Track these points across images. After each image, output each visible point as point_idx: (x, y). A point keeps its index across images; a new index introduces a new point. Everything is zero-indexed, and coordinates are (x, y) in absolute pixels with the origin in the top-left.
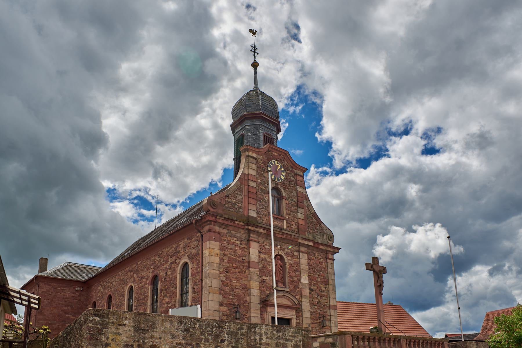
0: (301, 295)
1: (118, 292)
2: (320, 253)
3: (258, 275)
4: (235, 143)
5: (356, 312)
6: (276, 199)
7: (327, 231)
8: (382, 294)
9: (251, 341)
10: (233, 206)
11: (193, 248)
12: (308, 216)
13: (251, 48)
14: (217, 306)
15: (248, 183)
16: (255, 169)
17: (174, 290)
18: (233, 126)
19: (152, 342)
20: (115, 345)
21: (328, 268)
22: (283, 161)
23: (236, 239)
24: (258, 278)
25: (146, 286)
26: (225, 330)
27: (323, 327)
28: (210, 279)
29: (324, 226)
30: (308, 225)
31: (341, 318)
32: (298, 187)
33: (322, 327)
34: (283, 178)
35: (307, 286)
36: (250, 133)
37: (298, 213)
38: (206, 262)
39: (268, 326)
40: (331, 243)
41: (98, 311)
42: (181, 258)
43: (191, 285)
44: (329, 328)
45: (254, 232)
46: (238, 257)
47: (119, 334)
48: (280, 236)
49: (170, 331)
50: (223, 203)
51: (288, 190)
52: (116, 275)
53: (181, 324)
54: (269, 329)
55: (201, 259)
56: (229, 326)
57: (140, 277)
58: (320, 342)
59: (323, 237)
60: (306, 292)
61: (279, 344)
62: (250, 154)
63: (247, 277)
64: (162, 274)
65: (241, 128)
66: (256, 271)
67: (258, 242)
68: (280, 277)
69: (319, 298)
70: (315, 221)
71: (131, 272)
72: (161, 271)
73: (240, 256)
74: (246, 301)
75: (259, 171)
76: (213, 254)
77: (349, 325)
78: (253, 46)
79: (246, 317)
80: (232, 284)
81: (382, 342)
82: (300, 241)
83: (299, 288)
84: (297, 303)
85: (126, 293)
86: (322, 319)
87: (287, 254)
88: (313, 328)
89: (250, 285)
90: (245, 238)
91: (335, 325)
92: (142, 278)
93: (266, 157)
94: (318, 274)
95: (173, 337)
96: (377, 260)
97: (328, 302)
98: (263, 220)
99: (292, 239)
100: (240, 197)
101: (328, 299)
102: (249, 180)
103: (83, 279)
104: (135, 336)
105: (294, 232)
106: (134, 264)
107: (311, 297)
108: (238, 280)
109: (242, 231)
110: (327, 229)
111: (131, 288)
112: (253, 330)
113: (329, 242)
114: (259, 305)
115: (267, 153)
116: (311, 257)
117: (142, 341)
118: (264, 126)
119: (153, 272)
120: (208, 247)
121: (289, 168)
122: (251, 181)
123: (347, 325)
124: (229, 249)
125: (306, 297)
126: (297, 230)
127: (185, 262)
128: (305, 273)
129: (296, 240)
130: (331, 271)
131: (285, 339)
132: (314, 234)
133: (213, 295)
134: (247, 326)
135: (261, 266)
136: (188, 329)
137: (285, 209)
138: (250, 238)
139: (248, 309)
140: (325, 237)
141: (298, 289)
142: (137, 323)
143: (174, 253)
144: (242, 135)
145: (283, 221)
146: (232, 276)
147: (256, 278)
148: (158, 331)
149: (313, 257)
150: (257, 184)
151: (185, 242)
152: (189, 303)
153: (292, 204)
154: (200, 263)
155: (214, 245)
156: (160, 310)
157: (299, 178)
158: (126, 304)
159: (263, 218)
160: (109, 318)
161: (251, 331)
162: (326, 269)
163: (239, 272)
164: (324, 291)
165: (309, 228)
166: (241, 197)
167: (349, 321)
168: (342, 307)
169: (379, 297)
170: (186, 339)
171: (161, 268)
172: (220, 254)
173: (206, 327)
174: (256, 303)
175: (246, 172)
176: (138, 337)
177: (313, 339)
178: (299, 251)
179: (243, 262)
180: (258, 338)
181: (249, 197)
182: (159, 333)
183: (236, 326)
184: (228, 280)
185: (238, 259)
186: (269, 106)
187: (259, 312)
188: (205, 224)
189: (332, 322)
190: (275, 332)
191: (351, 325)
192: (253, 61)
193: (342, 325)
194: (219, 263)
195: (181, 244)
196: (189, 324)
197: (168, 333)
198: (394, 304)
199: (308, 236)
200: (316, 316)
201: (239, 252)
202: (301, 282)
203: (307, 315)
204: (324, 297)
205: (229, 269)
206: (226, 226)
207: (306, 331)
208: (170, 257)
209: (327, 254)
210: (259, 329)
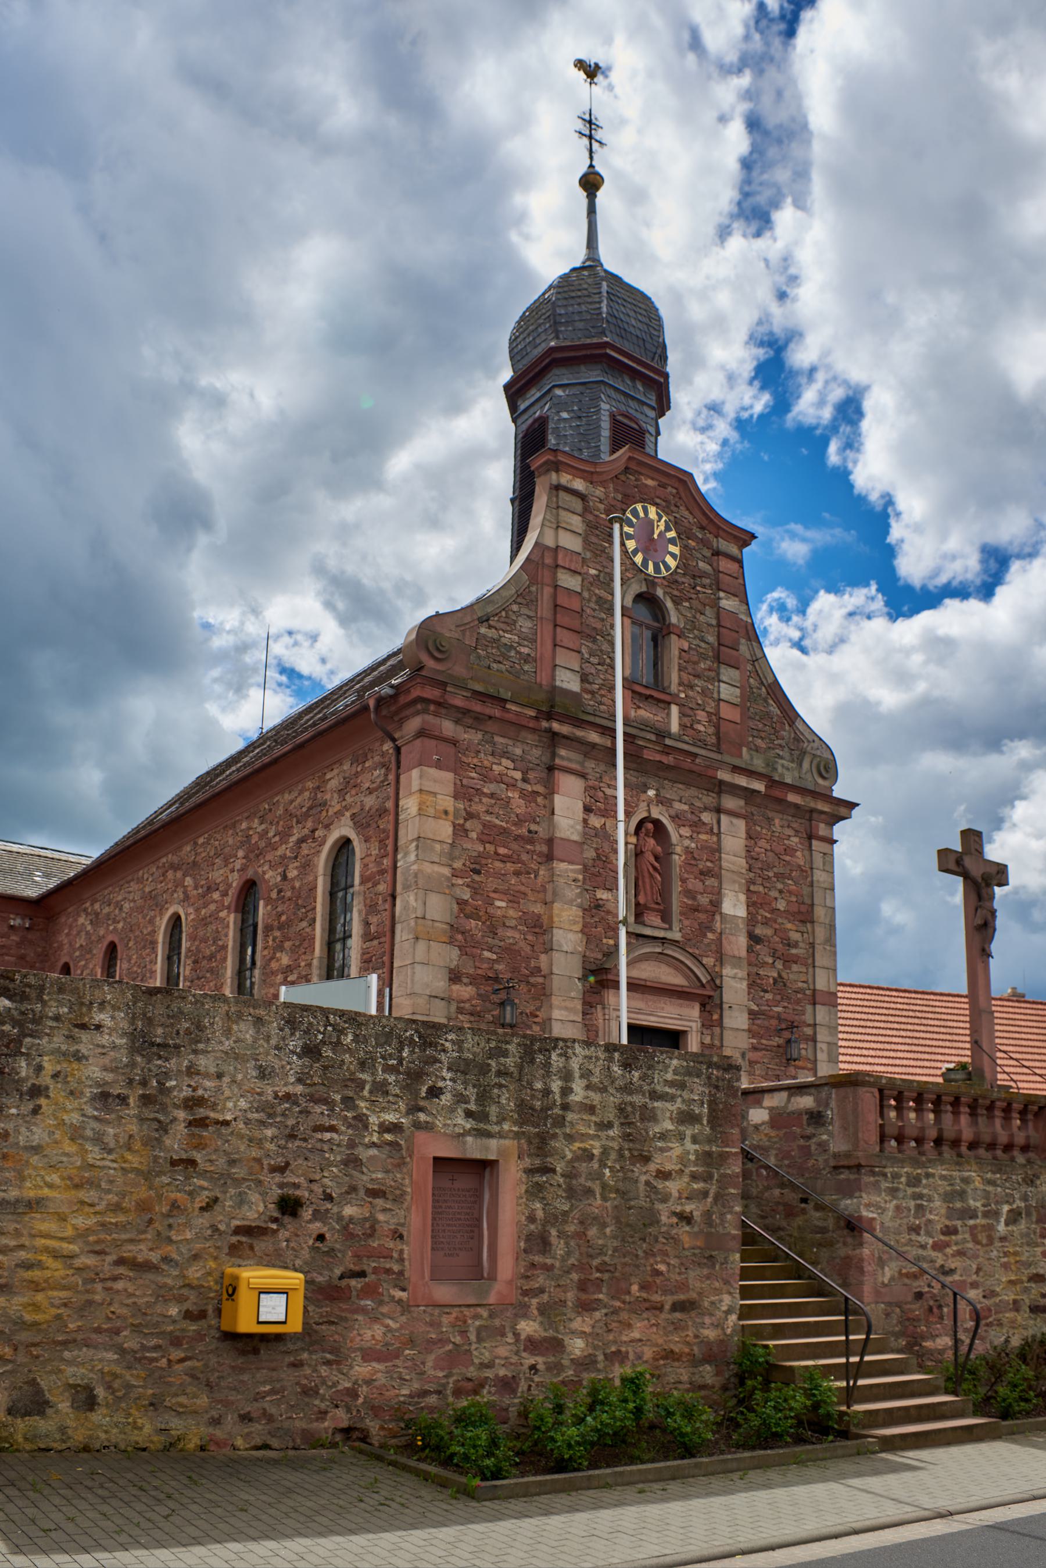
0: (722, 954)
1: (137, 933)
2: (790, 818)
3: (579, 884)
4: (519, 445)
5: (903, 1020)
6: (648, 634)
7: (815, 745)
8: (990, 955)
9: (533, 1097)
10: (503, 655)
11: (370, 791)
12: (753, 693)
13: (580, 125)
14: (442, 983)
15: (554, 578)
16: (580, 532)
17: (307, 930)
18: (514, 389)
19: (189, 1086)
20: (63, 1094)
21: (812, 868)
22: (673, 508)
23: (511, 765)
24: (581, 893)
25: (223, 914)
26: (443, 1057)
27: (788, 1060)
28: (421, 893)
29: (805, 727)
30: (751, 724)
31: (852, 1037)
32: (722, 594)
33: (784, 1061)
34: (672, 563)
35: (741, 926)
36: (568, 412)
37: (719, 681)
38: (410, 838)
39: (593, 1049)
40: (825, 787)
41: (8, 978)
42: (331, 824)
43: (360, 912)
44: (810, 1066)
45: (569, 742)
46: (515, 824)
47: (78, 1057)
48: (658, 757)
49: (253, 1051)
50: (470, 641)
51: (686, 604)
52: (133, 880)
53: (293, 1030)
54: (597, 1058)
55: (391, 827)
56: (459, 1044)
57: (202, 887)
58: (771, 1109)
59: (800, 765)
60: (738, 944)
61: (629, 1109)
62: (565, 479)
63: (544, 890)
64: (272, 876)
65: (538, 395)
66: (572, 871)
67: (583, 776)
68: (653, 893)
69: (779, 965)
70: (774, 709)
71: (175, 871)
72: (266, 868)
73: (520, 821)
74: (538, 969)
75: (594, 539)
76: (431, 811)
77: (877, 1060)
78: (587, 117)
79: (536, 1020)
80: (491, 910)
81: (982, 1115)
82: (723, 775)
83: (713, 931)
84: (704, 981)
85: (160, 939)
86: (786, 1035)
87: (677, 816)
88: (757, 1062)
89: (551, 918)
90: (537, 762)
91: (829, 1054)
92: (209, 888)
93: (616, 490)
94: (780, 886)
95: (263, 1074)
96: (977, 839)
97: (810, 981)
98: (601, 703)
99: (695, 768)
100: (525, 625)
101: (811, 970)
102: (557, 566)
103: (32, 893)
104: (133, 1064)
105: (705, 746)
106: (187, 843)
107: (753, 960)
108: (511, 898)
109: (531, 738)
110: (816, 739)
111: (176, 920)
112: (540, 1058)
113: (820, 781)
114: (579, 984)
115: (623, 477)
116: (758, 828)
117: (155, 1084)
118: (616, 389)
119: (243, 869)
120: (415, 786)
121: (695, 530)
122: (565, 571)
123: (870, 1060)
124: (485, 795)
125: (736, 961)
126: (713, 740)
127: (342, 837)
128: (734, 882)
129: (710, 773)
130: (821, 879)
131: (650, 1094)
132: (772, 753)
133: (429, 947)
134: (519, 1045)
135: (590, 854)
136: (316, 1046)
137: (676, 668)
138: (557, 761)
139: (543, 994)
140: (806, 765)
141: (710, 935)
142: (140, 1023)
143: (310, 808)
144: (540, 417)
145: (669, 709)
146: (492, 884)
147: (571, 892)
148: (213, 1051)
149: (764, 831)
150: (586, 582)
151: (344, 771)
152: (354, 971)
153: (702, 650)
154: (390, 842)
155: (435, 781)
156: (263, 992)
157: (725, 565)
158: (159, 971)
159: (603, 696)
160: (44, 1003)
161: (532, 1061)
162: (806, 872)
163: (517, 873)
164: (796, 945)
165: (755, 733)
166: (529, 624)
167: (879, 1046)
168: (859, 1003)
169: (980, 966)
170: (308, 1082)
171: (268, 858)
172: (456, 810)
173: (378, 1045)
174: (570, 977)
175: (549, 542)
176: (142, 1071)
177: (751, 1098)
178: (719, 810)
179: (531, 842)
180: (556, 1086)
181: (556, 625)
182: (216, 1058)
183: (482, 1044)
184: (478, 897)
185: (513, 828)
186: (633, 322)
187: (579, 1007)
188: (407, 712)
189: (819, 1045)
190: (616, 1069)
191: (884, 1061)
192: (583, 169)
193: (855, 1059)
194: (450, 841)
195: (330, 779)
196: (319, 1032)
197: (248, 1060)
198: (1027, 998)
199: (752, 759)
200: (766, 1023)
201: (519, 805)
202: (721, 913)
203: (736, 1020)
204: (796, 963)
205: (484, 861)
206: (478, 720)
207: (725, 1070)
208: (298, 822)
209: (810, 820)
210: (560, 1055)
